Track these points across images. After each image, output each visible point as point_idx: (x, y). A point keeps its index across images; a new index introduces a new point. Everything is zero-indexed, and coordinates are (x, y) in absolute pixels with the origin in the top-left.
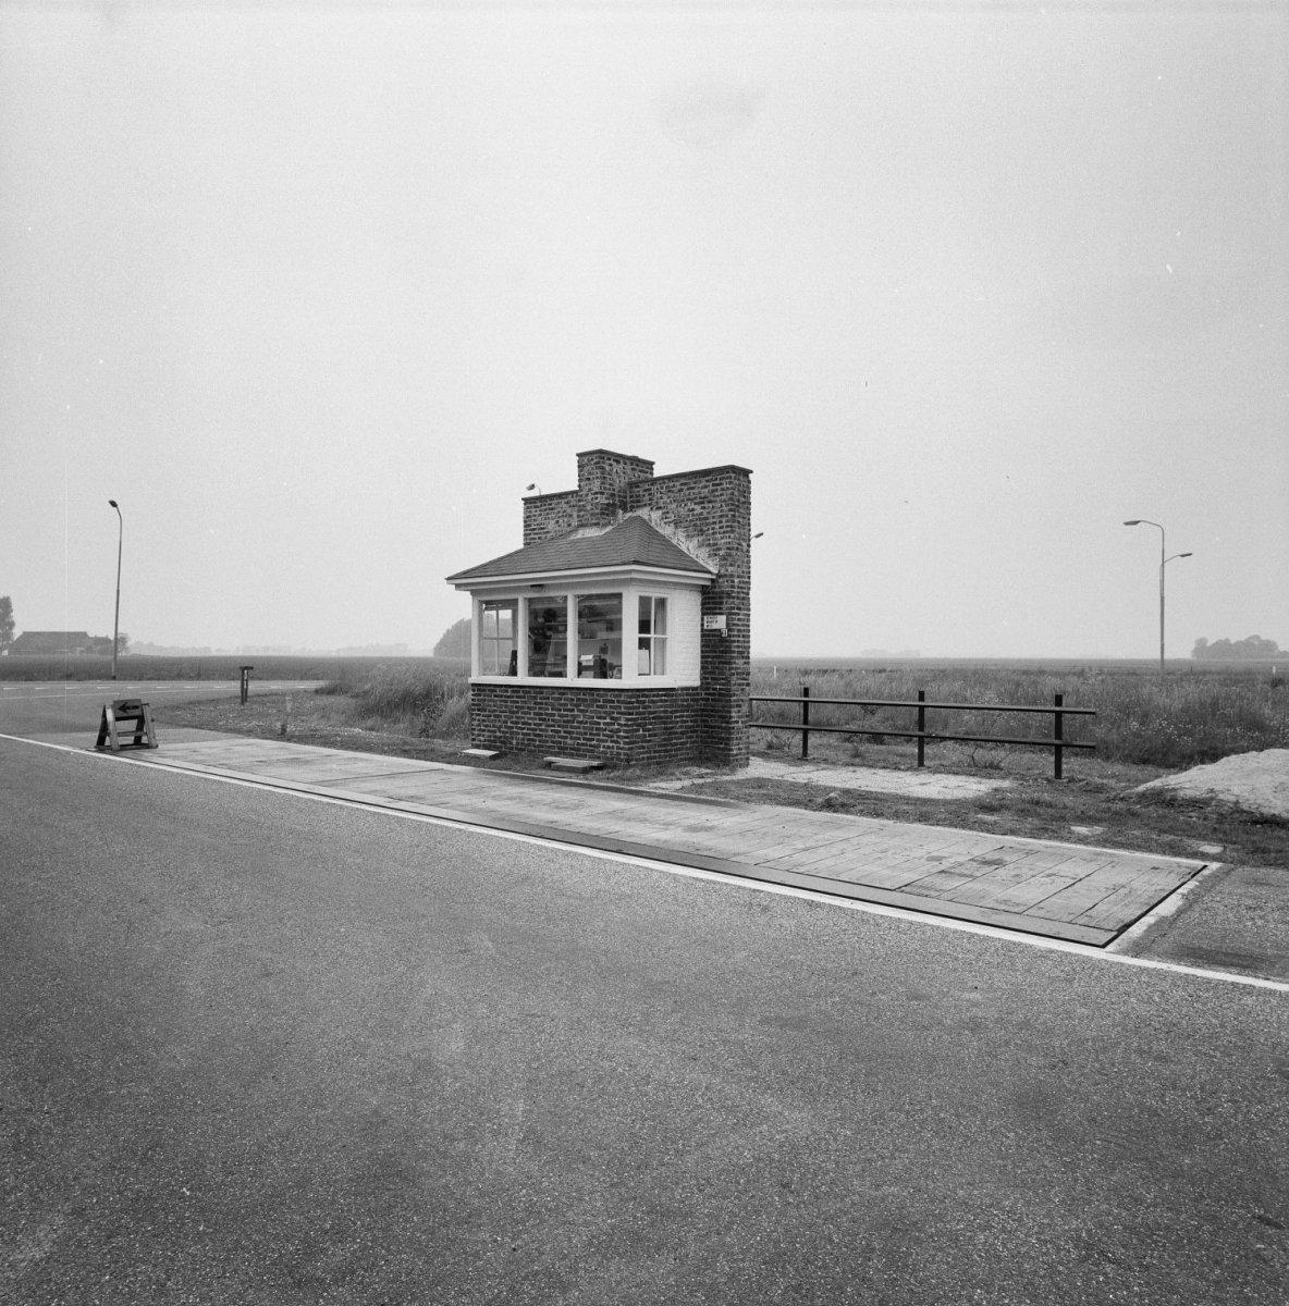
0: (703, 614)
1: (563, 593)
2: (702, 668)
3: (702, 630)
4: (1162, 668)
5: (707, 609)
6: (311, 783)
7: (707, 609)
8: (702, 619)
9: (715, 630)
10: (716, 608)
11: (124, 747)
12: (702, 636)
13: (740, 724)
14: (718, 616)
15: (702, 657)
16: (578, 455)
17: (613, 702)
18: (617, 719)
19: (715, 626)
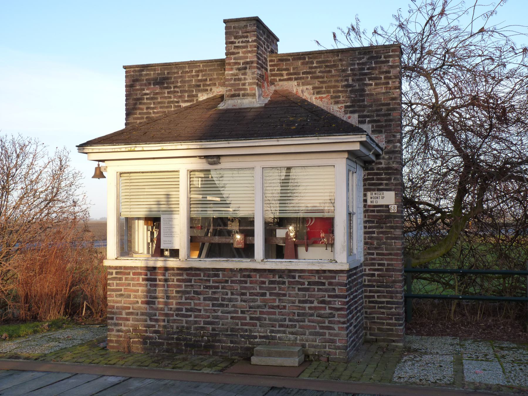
0: (366, 190)
1: (129, 271)
2: (366, 243)
3: (365, 206)
4: (14, 317)
5: (370, 184)
6: (51, 372)
7: (370, 184)
8: (365, 195)
9: (381, 206)
10: (381, 184)
11: (365, 201)
12: (365, 211)
13: (268, 296)
14: (385, 192)
15: (365, 233)
16: (225, 21)
17: (323, 284)
18: (329, 303)
19: (380, 202)
